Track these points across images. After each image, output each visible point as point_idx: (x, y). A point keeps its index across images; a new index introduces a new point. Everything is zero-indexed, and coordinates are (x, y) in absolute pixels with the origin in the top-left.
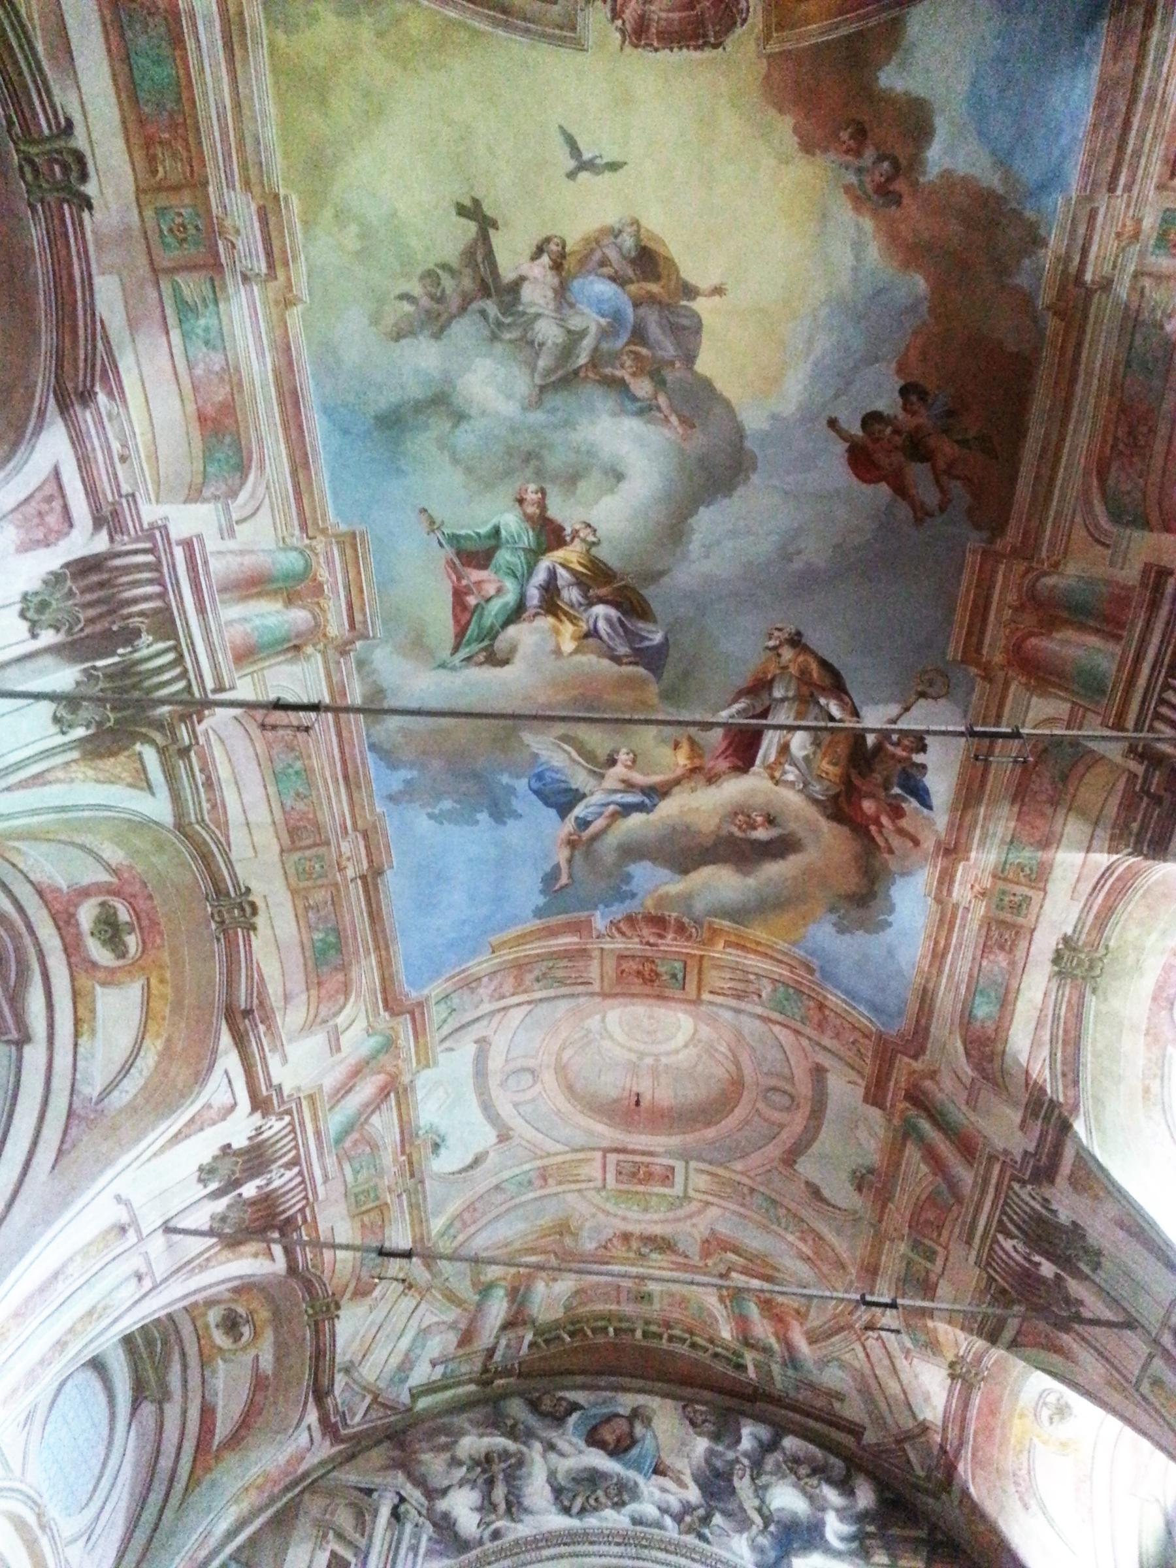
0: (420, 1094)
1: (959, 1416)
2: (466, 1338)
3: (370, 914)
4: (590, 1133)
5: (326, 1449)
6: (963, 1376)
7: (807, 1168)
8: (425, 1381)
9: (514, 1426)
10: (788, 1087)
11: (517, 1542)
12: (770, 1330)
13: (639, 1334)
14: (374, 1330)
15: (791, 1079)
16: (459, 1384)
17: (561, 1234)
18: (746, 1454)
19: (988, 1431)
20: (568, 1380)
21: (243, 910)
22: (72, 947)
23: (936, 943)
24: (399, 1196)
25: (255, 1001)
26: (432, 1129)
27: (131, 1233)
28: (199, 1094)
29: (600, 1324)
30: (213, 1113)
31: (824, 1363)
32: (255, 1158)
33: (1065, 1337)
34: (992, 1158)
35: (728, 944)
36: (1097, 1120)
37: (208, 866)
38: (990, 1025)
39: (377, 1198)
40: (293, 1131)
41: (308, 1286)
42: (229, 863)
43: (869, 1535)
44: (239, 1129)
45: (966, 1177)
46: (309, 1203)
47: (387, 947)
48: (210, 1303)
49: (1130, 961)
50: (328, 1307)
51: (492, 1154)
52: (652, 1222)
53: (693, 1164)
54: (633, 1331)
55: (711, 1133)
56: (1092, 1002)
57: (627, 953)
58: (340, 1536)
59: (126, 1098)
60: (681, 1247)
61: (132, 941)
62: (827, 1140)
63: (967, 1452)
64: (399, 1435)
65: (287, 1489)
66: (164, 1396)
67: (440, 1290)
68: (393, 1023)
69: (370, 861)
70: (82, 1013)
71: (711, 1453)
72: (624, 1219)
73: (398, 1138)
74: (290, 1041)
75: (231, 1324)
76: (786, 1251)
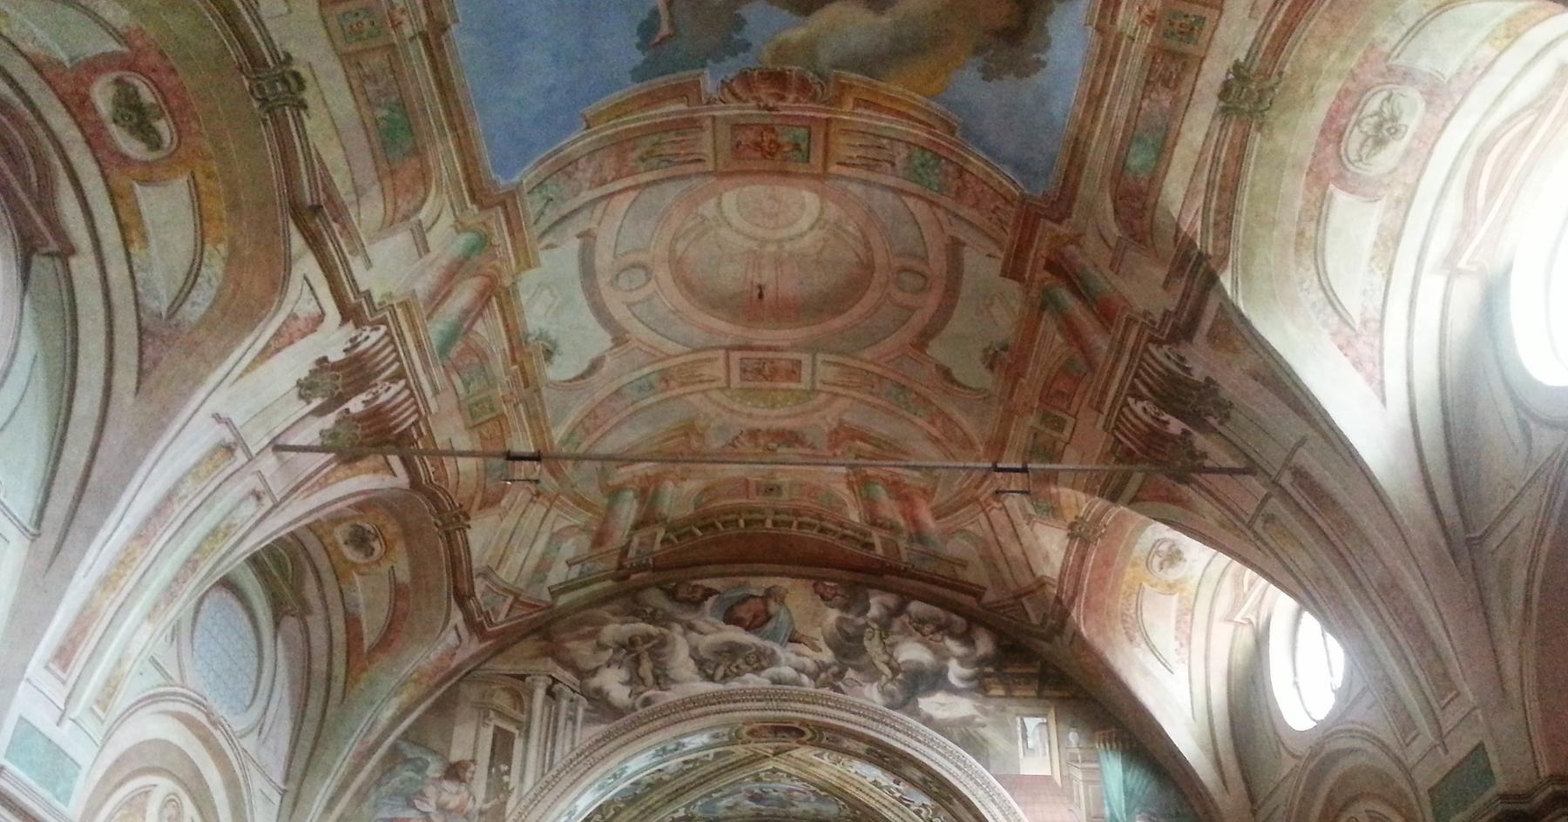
0: (524, 298)
1: (1074, 570)
2: (599, 540)
3: (440, 84)
4: (710, 331)
5: (474, 646)
6: (1081, 535)
7: (938, 351)
8: (562, 579)
9: (653, 614)
10: (920, 267)
11: (667, 706)
12: (896, 509)
13: (769, 524)
14: (507, 537)
15: (924, 259)
16: (598, 580)
17: (686, 435)
18: (875, 620)
19: (1100, 582)
20: (700, 570)
21: (285, 82)
22: (95, 140)
23: (1094, 82)
24: (515, 406)
25: (323, 196)
26: (542, 336)
27: (239, 453)
28: (281, 302)
29: (731, 517)
30: (301, 324)
31: (949, 534)
32: (355, 372)
33: (1184, 488)
34: (1130, 321)
35: (858, 103)
36: (1245, 270)
37: (233, 25)
38: (1144, 176)
39: (492, 409)
40: (392, 341)
41: (432, 497)
42: (259, 22)
43: (988, 675)
44: (333, 341)
45: (1101, 343)
46: (422, 417)
47: (464, 125)
48: (336, 520)
49: (1303, 90)
50: (457, 517)
51: (608, 359)
52: (780, 417)
53: (820, 357)
54: (763, 522)
55: (837, 323)
56: (1257, 140)
57: (742, 121)
58: (501, 714)
59: (201, 310)
60: (809, 439)
61: (163, 126)
62: (959, 322)
63: (1081, 601)
64: (545, 628)
65: (439, 685)
66: (304, 610)
67: (568, 496)
68: (483, 217)
69: (429, 14)
70: (125, 218)
71: (840, 620)
72: (750, 416)
73: (506, 346)
74: (372, 241)
75: (360, 540)
76: (914, 435)
